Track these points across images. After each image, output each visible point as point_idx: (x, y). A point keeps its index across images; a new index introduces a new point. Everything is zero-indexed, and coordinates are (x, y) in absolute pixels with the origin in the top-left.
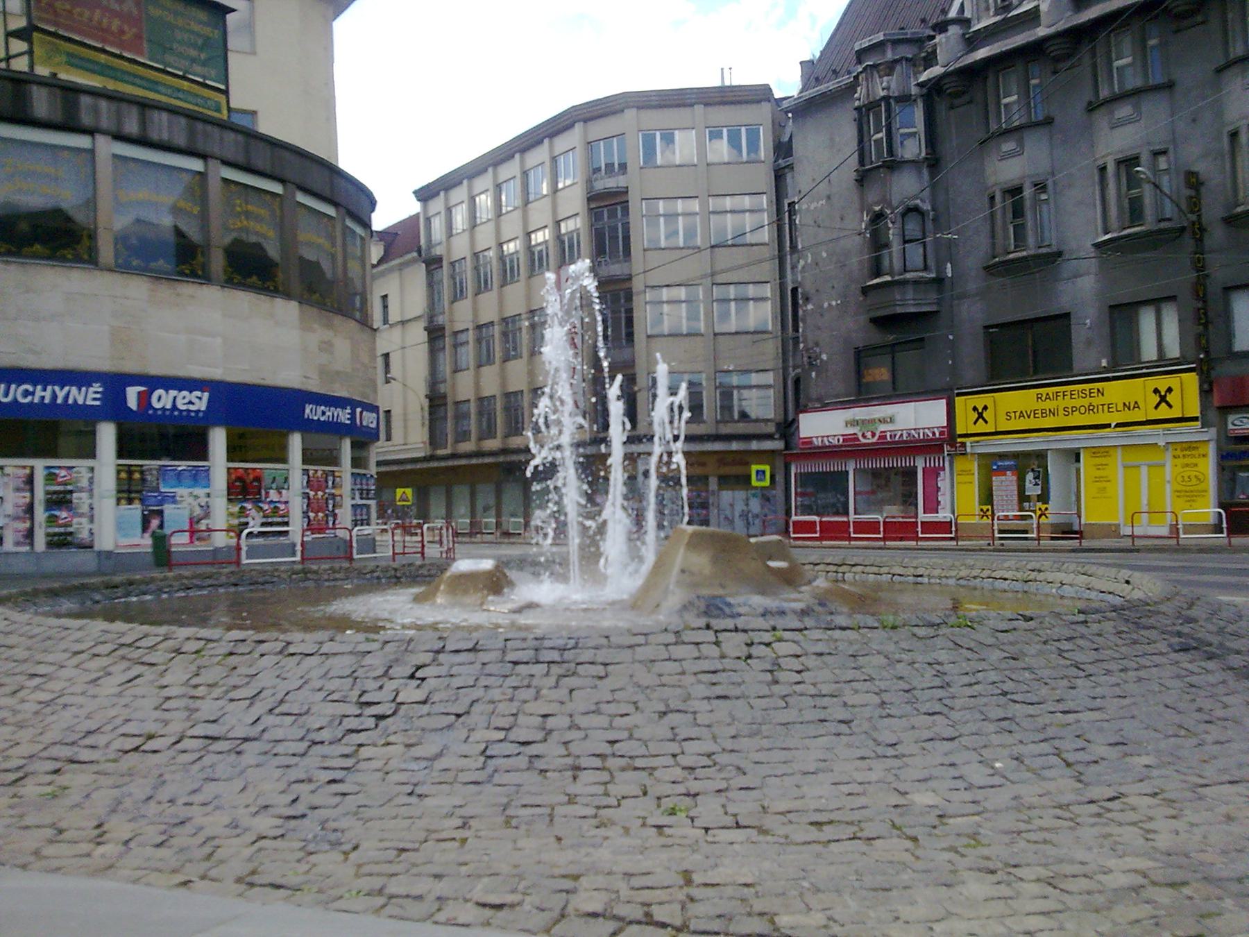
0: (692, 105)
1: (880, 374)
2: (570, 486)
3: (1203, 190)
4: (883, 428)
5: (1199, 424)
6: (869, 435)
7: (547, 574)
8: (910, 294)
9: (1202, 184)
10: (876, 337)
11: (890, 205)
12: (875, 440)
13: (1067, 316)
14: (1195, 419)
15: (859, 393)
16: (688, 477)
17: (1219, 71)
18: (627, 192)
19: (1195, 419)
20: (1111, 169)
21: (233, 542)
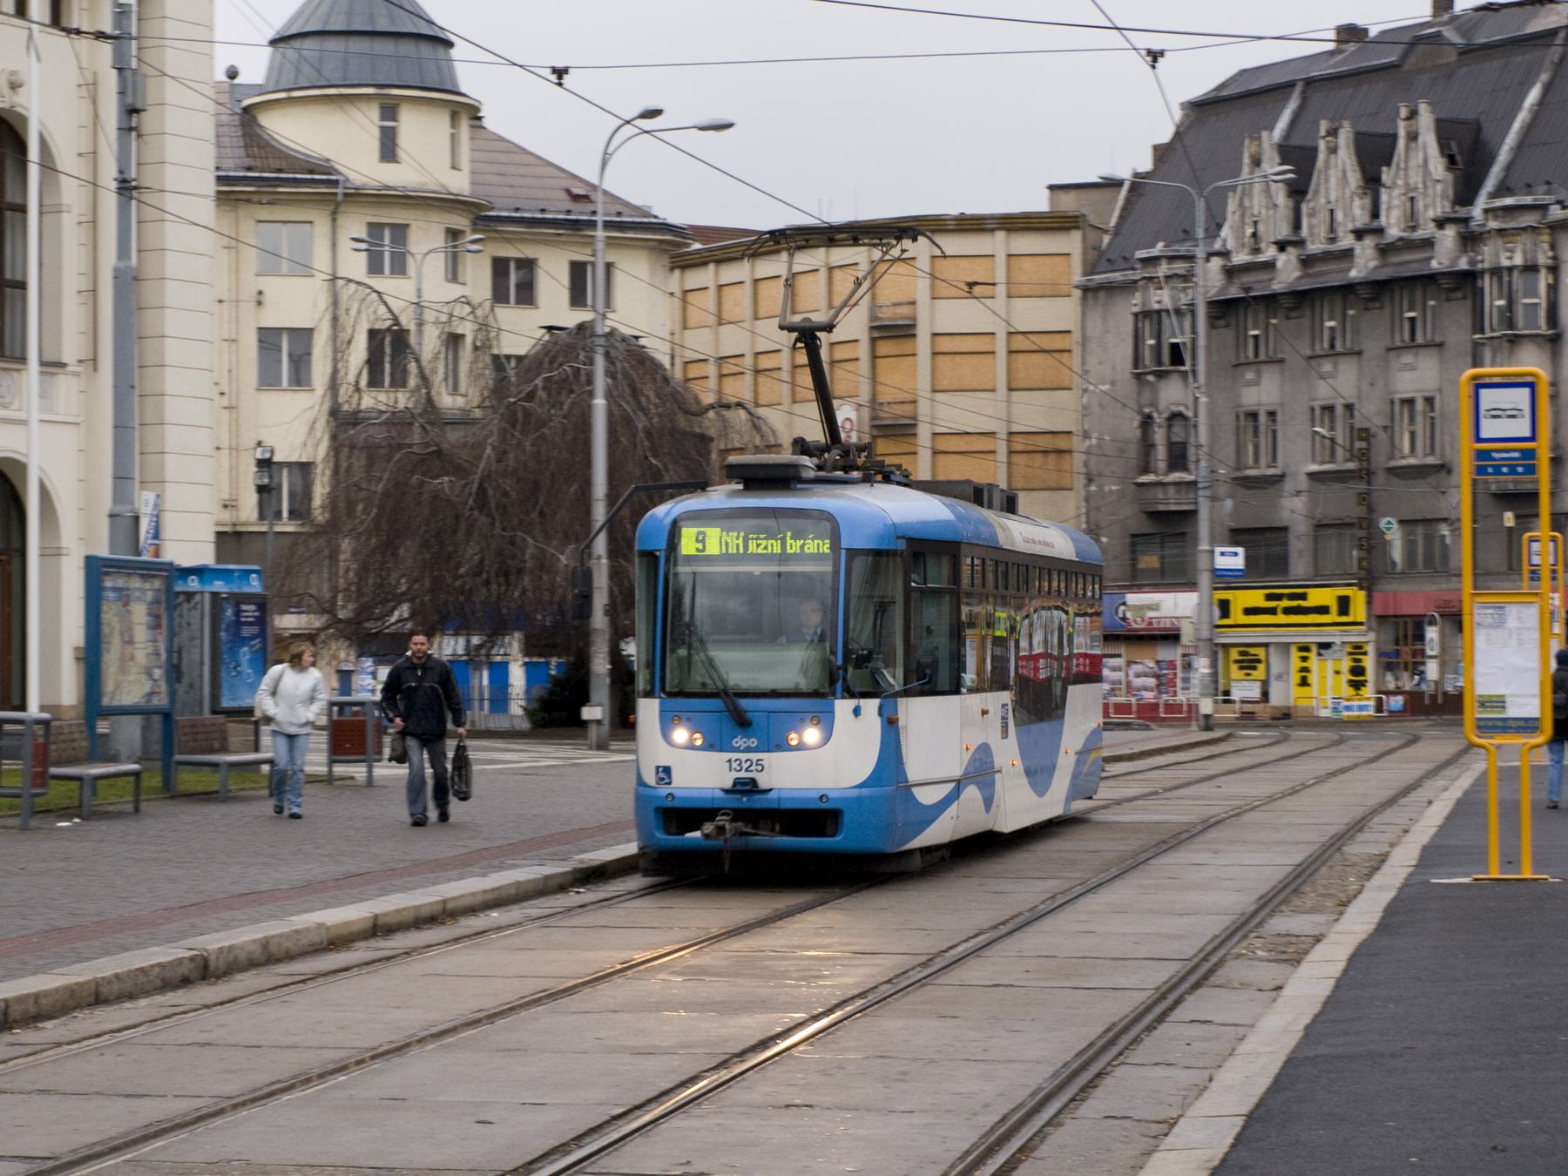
0: (992, 230)
1: (1150, 561)
2: (476, 704)
3: (1373, 441)
4: (1151, 614)
5: (1363, 628)
6: (1139, 620)
7: (1473, 224)
8: (1171, 491)
9: (1374, 436)
10: (1146, 527)
11: (1157, 410)
12: (1143, 626)
13: (1285, 529)
14: (1361, 624)
15: (1134, 578)
16: (280, 350)
17: (1389, 350)
18: (913, 326)
19: (1361, 624)
20: (1318, 412)
21: (124, 751)
